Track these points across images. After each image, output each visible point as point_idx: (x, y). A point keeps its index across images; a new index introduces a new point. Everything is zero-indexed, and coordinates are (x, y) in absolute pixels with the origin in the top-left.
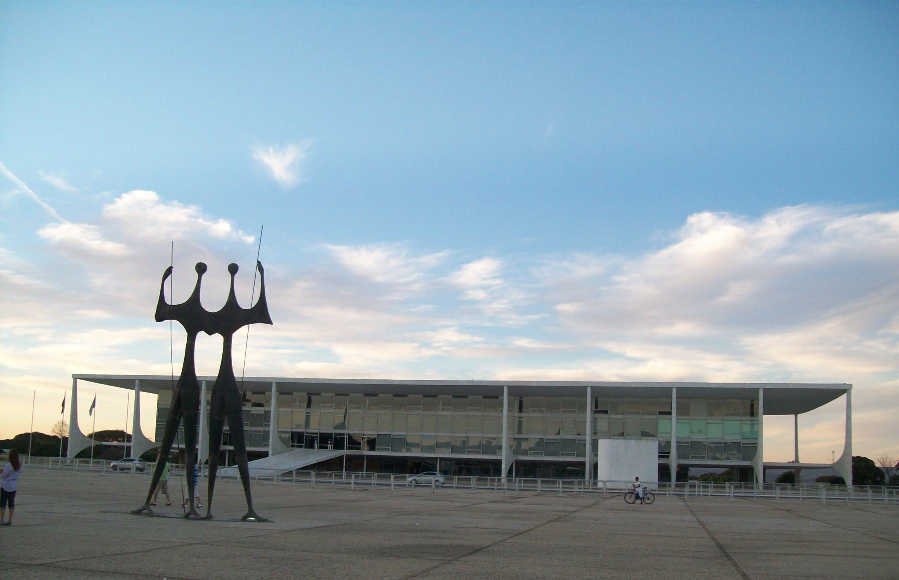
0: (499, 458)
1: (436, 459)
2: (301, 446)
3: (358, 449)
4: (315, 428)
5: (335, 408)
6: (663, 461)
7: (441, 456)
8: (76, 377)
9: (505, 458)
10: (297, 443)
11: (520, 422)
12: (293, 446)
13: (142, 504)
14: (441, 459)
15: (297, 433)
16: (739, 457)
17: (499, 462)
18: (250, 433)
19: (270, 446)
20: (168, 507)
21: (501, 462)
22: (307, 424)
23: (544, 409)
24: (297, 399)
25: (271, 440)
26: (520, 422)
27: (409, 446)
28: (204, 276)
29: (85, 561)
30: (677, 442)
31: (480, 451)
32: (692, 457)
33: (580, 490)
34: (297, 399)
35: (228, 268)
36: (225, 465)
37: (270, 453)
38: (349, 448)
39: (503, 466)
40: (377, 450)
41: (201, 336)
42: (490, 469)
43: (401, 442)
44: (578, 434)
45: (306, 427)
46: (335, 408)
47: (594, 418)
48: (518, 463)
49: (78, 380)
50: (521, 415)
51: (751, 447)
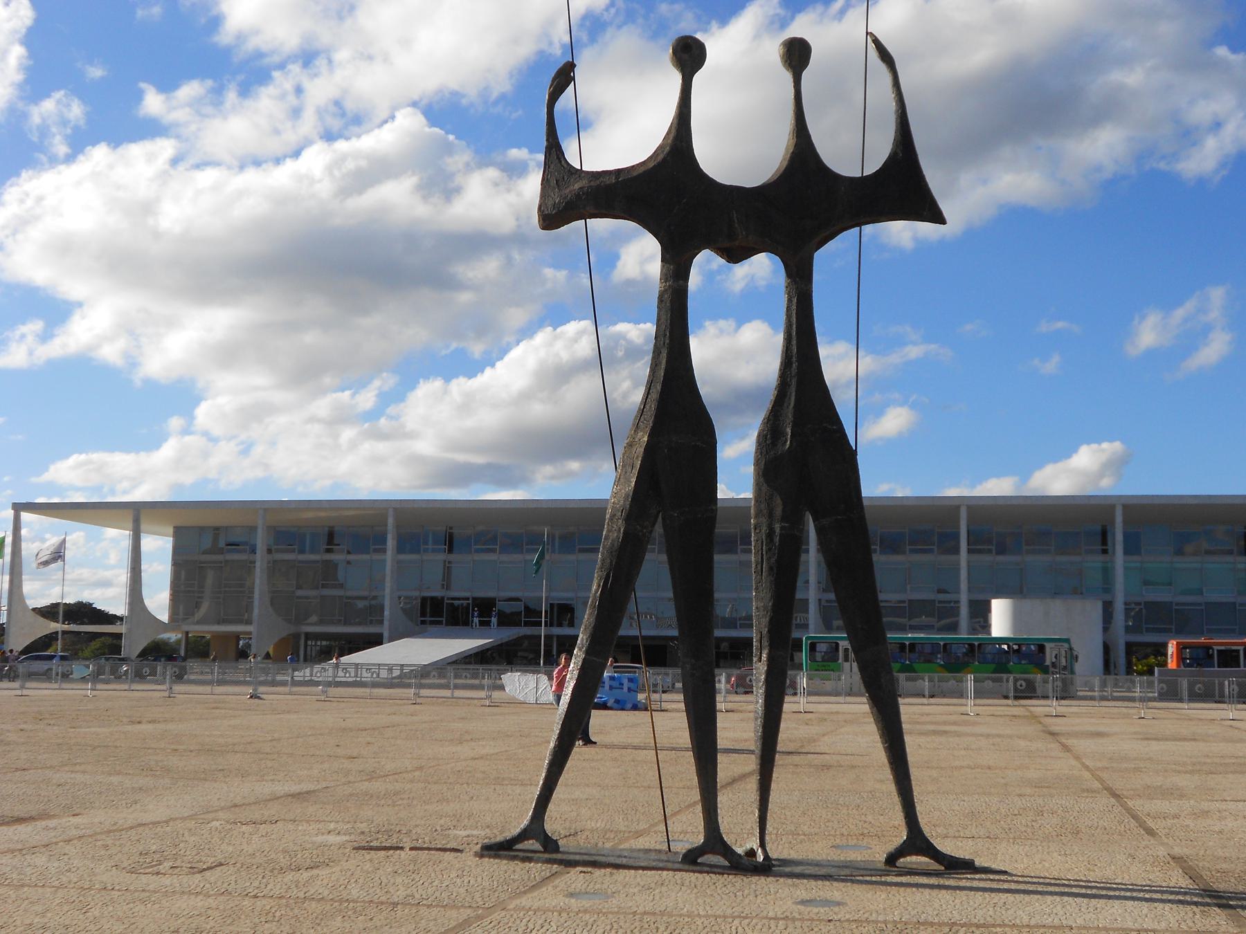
2: (440, 623)
4: (462, 590)
5: (500, 553)
8: (18, 508)
10: (430, 617)
12: (423, 622)
15: (432, 598)
16: (341, 620)
18: (1175, 607)
19: (386, 623)
21: (382, 638)
22: (447, 583)
23: (935, 548)
24: (430, 539)
25: (256, 612)
29: (1115, 879)
30: (1126, 604)
31: (1171, 629)
33: (1231, 697)
34: (430, 539)
36: (298, 660)
37: (386, 635)
40: (740, 627)
41: (705, 263)
44: (940, 591)
46: (500, 553)
47: (948, 543)
49: (26, 516)
50: (452, 557)
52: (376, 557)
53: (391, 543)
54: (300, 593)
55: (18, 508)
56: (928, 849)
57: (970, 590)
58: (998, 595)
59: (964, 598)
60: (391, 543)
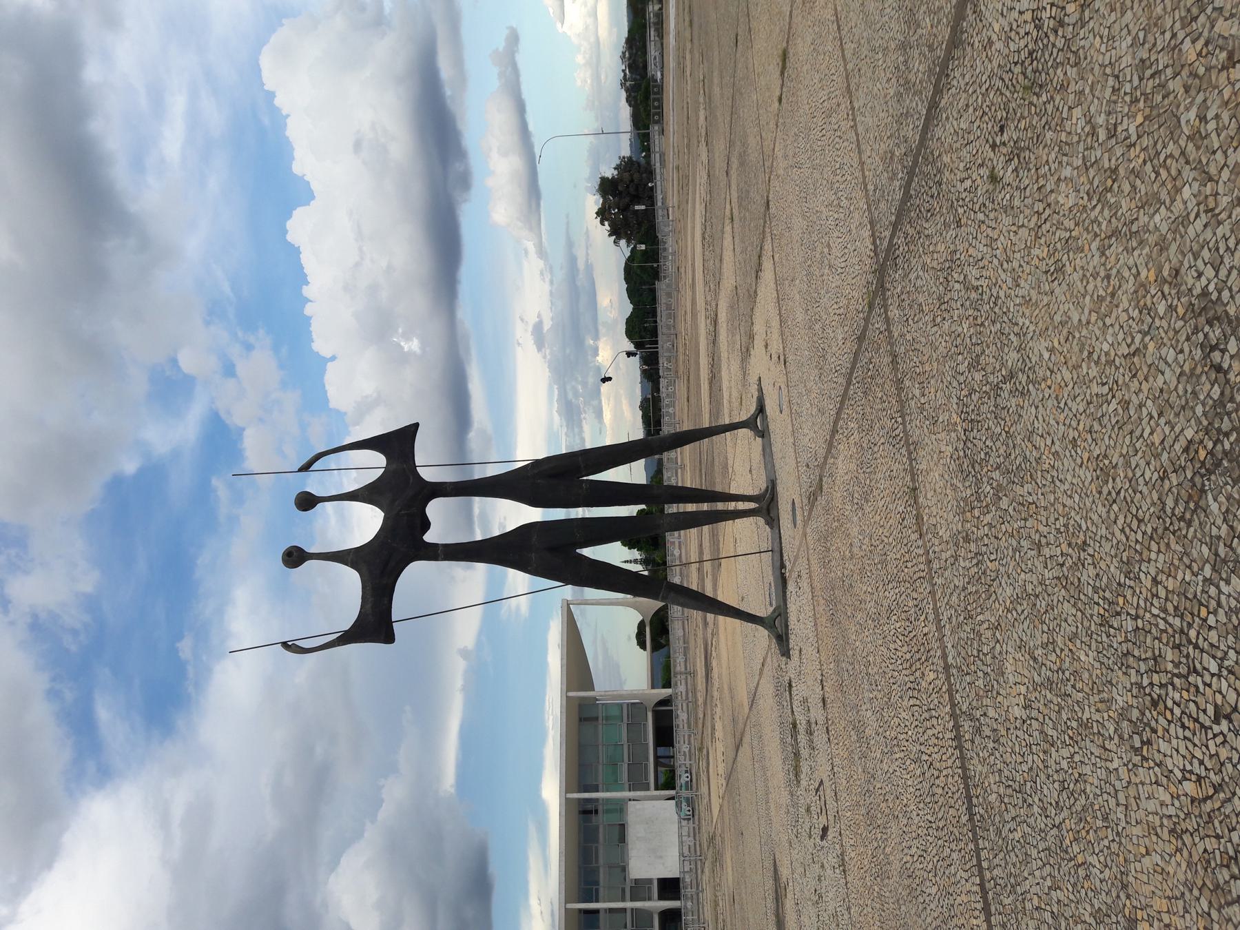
41: (429, 537)
51: (635, 709)
52: (627, 786)
56: (754, 417)
57: (623, 900)
59: (629, 905)
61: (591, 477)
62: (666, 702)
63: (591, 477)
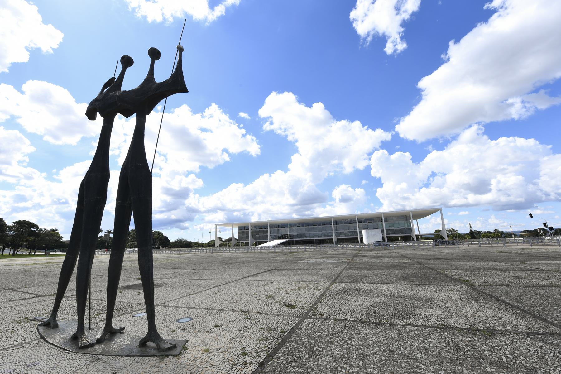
0: (332, 238)
1: (314, 239)
3: (293, 238)
6: (362, 237)
7: (315, 238)
9: (334, 238)
11: (337, 228)
13: (376, 152)
14: (315, 239)
17: (333, 239)
20: (174, 329)
25: (268, 238)
26: (337, 228)
27: (306, 237)
28: (128, 69)
32: (401, 234)
35: (148, 53)
38: (290, 238)
39: (334, 240)
41: (119, 119)
42: (331, 241)
43: (303, 236)
45: (278, 233)
48: (338, 239)
51: (410, 230)
53: (269, 227)
54: (256, 235)
55: (216, 225)
58: (364, 229)
59: (358, 230)
60: (269, 227)
61: (132, 217)
62: (413, 240)
63: (132, 217)
